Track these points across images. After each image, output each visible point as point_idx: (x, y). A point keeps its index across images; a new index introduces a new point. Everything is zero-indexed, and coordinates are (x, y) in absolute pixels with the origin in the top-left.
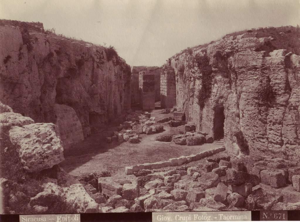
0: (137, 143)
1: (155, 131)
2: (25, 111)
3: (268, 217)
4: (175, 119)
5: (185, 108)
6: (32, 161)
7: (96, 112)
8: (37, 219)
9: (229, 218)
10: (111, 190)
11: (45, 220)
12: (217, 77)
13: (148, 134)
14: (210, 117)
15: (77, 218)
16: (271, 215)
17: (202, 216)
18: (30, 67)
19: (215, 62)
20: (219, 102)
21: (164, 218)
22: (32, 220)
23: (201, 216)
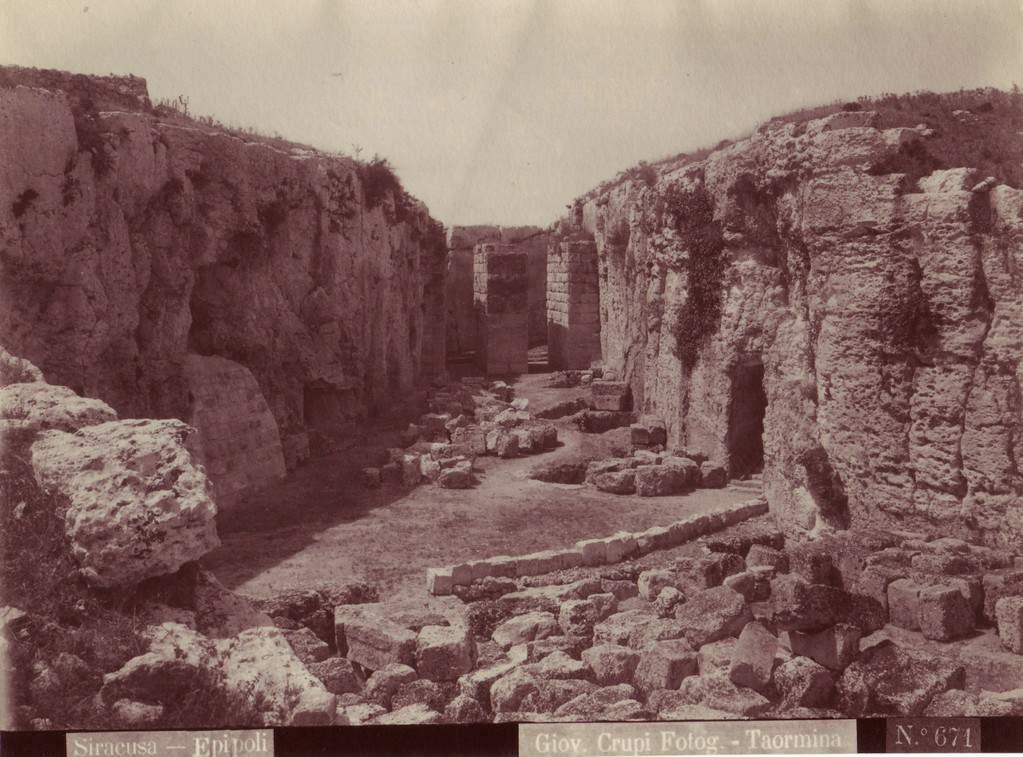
0: (466, 488)
1: (529, 446)
2: (85, 379)
3: (913, 741)
4: (598, 407)
5: (630, 367)
6: (110, 549)
7: (326, 383)
8: (126, 748)
9: (782, 743)
10: (378, 649)
11: (152, 750)
12: (741, 261)
13: (506, 457)
14: (717, 398)
15: (264, 744)
16: (924, 732)
17: (690, 738)
18: (102, 230)
19: (732, 211)
20: (748, 348)
21: (560, 744)
22: (109, 752)
23: (687, 737)
